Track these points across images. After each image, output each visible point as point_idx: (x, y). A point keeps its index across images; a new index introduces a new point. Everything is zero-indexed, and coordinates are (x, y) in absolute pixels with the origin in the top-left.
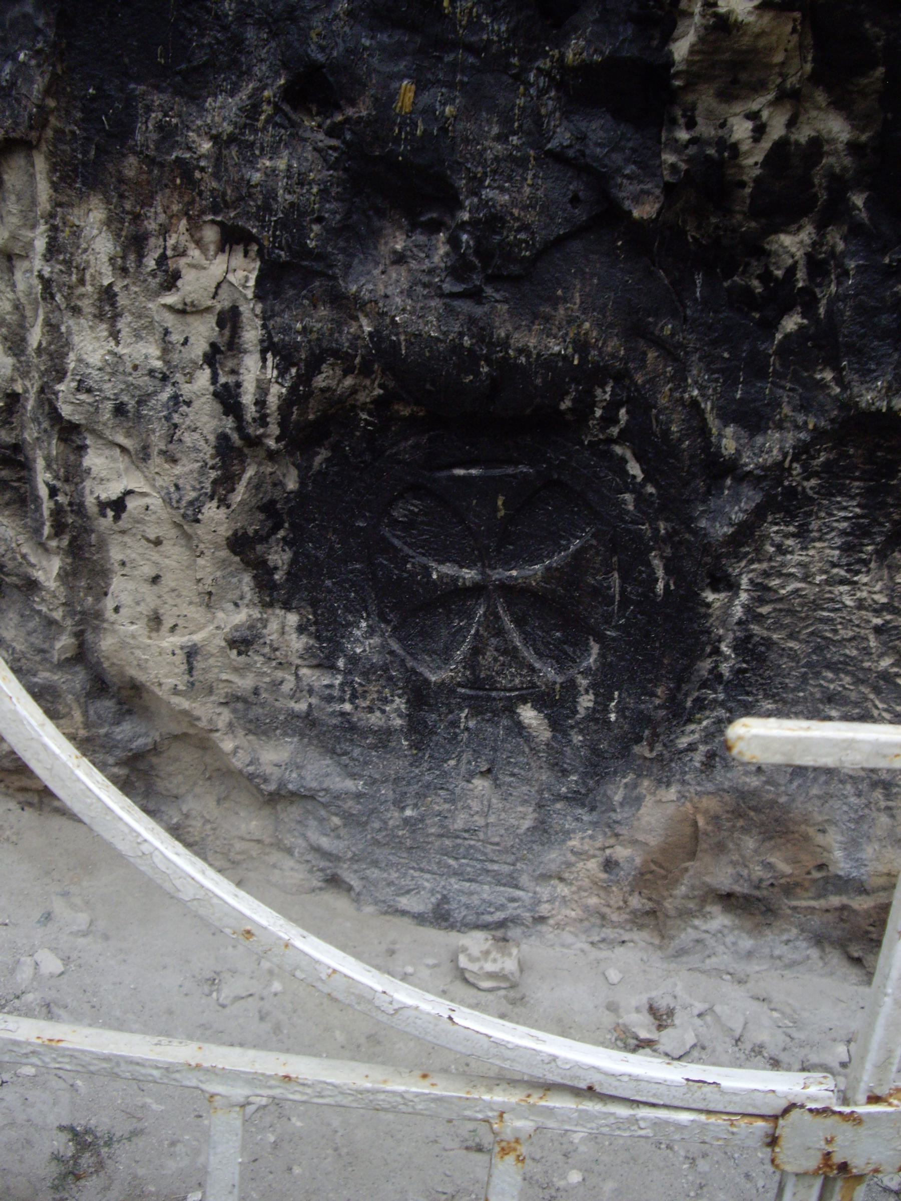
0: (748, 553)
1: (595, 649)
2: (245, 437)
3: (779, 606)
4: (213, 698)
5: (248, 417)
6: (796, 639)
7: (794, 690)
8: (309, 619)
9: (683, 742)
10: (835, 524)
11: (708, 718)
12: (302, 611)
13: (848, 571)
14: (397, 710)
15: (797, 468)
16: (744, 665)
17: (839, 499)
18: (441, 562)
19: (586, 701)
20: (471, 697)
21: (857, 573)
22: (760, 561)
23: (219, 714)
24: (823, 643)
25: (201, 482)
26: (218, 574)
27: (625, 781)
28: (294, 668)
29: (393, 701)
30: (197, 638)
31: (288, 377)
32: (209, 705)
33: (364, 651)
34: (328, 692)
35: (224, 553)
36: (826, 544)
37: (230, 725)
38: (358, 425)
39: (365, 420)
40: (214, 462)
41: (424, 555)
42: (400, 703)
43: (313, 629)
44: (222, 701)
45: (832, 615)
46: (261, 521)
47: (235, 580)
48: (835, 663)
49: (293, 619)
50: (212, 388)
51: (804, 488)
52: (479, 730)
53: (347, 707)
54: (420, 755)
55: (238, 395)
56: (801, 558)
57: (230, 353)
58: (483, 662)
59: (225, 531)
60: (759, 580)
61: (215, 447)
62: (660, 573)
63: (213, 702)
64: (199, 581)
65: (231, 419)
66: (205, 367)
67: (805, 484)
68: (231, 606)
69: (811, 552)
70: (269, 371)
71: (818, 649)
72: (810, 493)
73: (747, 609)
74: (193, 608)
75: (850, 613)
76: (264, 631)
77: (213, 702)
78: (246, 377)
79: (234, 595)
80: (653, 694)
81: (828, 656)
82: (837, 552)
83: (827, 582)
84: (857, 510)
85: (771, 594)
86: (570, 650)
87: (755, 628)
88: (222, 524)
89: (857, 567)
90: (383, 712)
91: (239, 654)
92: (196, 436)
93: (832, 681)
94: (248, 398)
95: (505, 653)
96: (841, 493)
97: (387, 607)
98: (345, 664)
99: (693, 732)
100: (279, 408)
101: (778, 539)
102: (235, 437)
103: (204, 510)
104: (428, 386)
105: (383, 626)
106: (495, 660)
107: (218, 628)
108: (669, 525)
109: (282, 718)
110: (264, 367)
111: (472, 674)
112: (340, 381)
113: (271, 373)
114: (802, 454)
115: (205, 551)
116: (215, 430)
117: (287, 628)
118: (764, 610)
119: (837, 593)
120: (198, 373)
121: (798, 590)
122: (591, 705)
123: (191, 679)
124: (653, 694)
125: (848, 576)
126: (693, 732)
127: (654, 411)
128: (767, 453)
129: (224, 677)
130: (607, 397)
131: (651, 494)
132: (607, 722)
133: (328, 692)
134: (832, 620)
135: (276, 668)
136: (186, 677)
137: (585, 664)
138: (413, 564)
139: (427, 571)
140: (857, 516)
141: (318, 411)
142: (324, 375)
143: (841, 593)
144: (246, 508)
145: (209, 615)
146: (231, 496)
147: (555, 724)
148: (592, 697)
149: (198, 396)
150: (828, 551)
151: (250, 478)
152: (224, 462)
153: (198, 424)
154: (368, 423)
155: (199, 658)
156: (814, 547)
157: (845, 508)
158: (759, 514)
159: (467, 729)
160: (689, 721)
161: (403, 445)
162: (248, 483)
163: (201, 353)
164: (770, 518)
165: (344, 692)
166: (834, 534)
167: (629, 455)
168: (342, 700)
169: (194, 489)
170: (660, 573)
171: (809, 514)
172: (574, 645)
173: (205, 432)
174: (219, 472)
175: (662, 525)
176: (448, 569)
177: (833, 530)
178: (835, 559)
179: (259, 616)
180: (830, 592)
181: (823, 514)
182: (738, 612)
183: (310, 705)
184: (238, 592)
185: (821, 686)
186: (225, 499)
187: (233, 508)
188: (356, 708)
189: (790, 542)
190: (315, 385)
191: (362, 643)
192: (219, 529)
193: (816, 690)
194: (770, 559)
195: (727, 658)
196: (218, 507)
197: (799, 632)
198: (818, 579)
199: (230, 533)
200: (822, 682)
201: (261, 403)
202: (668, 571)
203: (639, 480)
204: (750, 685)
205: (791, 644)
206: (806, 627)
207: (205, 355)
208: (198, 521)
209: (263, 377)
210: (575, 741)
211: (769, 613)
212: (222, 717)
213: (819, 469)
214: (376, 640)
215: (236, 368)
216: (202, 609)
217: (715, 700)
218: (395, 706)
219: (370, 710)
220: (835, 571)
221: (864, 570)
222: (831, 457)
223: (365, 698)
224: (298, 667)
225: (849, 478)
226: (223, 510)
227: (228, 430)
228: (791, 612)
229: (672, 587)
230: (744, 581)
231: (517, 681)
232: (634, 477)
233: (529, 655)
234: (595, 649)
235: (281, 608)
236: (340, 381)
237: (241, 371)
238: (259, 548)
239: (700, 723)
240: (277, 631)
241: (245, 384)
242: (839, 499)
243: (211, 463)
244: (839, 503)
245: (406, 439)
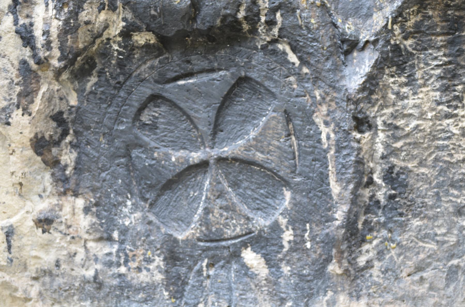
0: (377, 100)
2: (39, 63)
3: (408, 141)
4: (27, 273)
5: (39, 45)
6: (425, 166)
7: (432, 207)
8: (91, 202)
9: (362, 261)
10: (432, 72)
11: (376, 237)
12: (86, 196)
13: (448, 107)
14: (158, 267)
15: (397, 29)
16: (393, 192)
17: (430, 51)
18: (178, 150)
19: (288, 236)
20: (208, 249)
21: (456, 107)
22: (387, 107)
23: (32, 286)
24: (445, 166)
25: (10, 95)
26: (26, 170)
27: (326, 298)
28: (83, 242)
29: (154, 260)
30: (13, 221)
31: (62, 14)
32: (24, 279)
33: (131, 223)
34: (108, 258)
35: (30, 152)
36: (429, 88)
37: (40, 294)
38: (113, 56)
39: (117, 50)
40: (18, 80)
41: (165, 146)
42: (159, 261)
43: (94, 209)
44: (34, 275)
45: (446, 142)
46: (54, 128)
47: (39, 177)
48: (457, 181)
49: (80, 202)
50: (14, 28)
51: (405, 46)
52: (216, 276)
53: (123, 270)
54: (178, 302)
55: (31, 31)
56: (414, 101)
57: (25, 4)
59: (29, 134)
60: (390, 122)
61: (19, 70)
63: (27, 276)
64: (13, 173)
65: (28, 49)
66: (10, 14)
67: (405, 42)
68: (37, 198)
69: (421, 96)
70: (50, 11)
71: (443, 171)
72: (410, 49)
73: (387, 146)
74: (9, 197)
75: (458, 140)
76: (61, 213)
77: (27, 276)
78: (36, 20)
79: (39, 189)
81: (451, 176)
82: (438, 93)
83: (436, 117)
84: (445, 59)
85: (400, 132)
87: (393, 160)
88: (26, 128)
89: (454, 103)
90: (148, 270)
91: (44, 232)
92: (5, 61)
93: (457, 197)
94: (38, 32)
95: (226, 209)
96: (431, 47)
97: (144, 188)
98: (119, 236)
99: (367, 251)
100: (58, 36)
101: (396, 88)
102: (31, 62)
103: (13, 115)
104: (153, 12)
105: (142, 203)
106: (221, 215)
107: (27, 212)
108: (321, 90)
109: (77, 284)
110: (47, 10)
111: (207, 229)
112: (97, 16)
113: (52, 12)
115: (16, 149)
116: (18, 57)
117: (76, 210)
118: (399, 145)
119: (445, 125)
120: (5, 18)
121: (418, 126)
122: (292, 238)
123: (10, 256)
125: (450, 111)
126: (367, 251)
127: (298, 11)
128: (376, 25)
129: (34, 253)
130: (267, 5)
131: (306, 74)
132: (306, 250)
133: (108, 258)
134: (447, 146)
135: (70, 243)
136: (6, 254)
137: (283, 208)
138: (158, 153)
139: (167, 157)
140: (446, 64)
141: (85, 41)
142: (86, 12)
143: (448, 125)
144: (43, 116)
145: (22, 203)
146: (31, 106)
147: (269, 262)
148: (291, 232)
149: (5, 33)
150: (432, 93)
151: (44, 93)
152: (25, 81)
153: (6, 53)
154: (120, 53)
155: (15, 237)
156: (422, 92)
157: (436, 58)
158: (379, 66)
159: (208, 277)
160: (363, 241)
161: (143, 68)
162: (43, 97)
163: (6, 6)
164: (387, 71)
165: (120, 257)
166: (432, 80)
167: (288, 49)
168: (119, 265)
169: (5, 100)
171: (412, 66)
172: (274, 197)
173: (11, 59)
174: (22, 88)
176: (182, 153)
177: (431, 77)
178: (438, 98)
179: (57, 202)
180: (441, 125)
181: (422, 65)
182: (380, 149)
183: (96, 270)
184: (42, 187)
185: (451, 201)
186: (27, 108)
187: (34, 115)
188: (129, 269)
189: (405, 90)
190: (80, 19)
191: (129, 218)
192: (24, 131)
193: (448, 205)
194: (394, 105)
195: (380, 187)
196: (23, 115)
197: (426, 160)
198: (430, 115)
199: (32, 135)
200: (451, 198)
201: (46, 33)
203: (297, 65)
204: (401, 207)
205: (423, 170)
206: (430, 155)
207: (10, 6)
208: (8, 124)
209: (47, 16)
210: (286, 272)
211: (402, 147)
212: (34, 288)
213: (412, 30)
214: (138, 215)
215: (30, 14)
216: (16, 198)
217: (378, 223)
218: (155, 264)
219: (139, 269)
220: (440, 107)
221: (460, 105)
222: (418, 20)
223: (134, 260)
224: (86, 241)
225: (433, 34)
226: (26, 117)
227: (26, 58)
228: (416, 144)
230: (379, 122)
231: (238, 229)
232: (294, 64)
233: (244, 209)
234: (288, 194)
235: (72, 196)
236: (97, 16)
237: (33, 16)
238: (55, 150)
239: (371, 242)
240: (69, 213)
241: (36, 24)
242: (430, 51)
243: (16, 81)
244: (431, 54)
245: (145, 63)
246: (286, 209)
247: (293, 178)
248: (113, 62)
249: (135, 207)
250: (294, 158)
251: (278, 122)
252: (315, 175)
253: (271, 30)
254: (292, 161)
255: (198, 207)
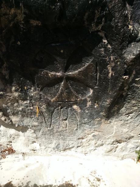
1: (91, 91)
18: (51, 72)
19: (89, 104)
33: (34, 95)
53: (32, 108)
58: (63, 96)
62: (110, 71)
80: (106, 101)
86: (85, 92)
114: (127, 65)
122: (90, 104)
124: (106, 101)
127: (113, 19)
131: (109, 48)
137: (89, 95)
139: (47, 74)
148: (91, 102)
154: (24, 29)
170: (110, 71)
175: (112, 57)
183: (22, 108)
202: (112, 70)
214: (37, 92)
229: (113, 75)
246: (90, 96)
247: (95, 86)
248: (21, 33)
249: (35, 90)
250: (97, 80)
251: (93, 67)
252: (109, 36)
253: (98, 26)
254: (96, 81)
255: (59, 91)
